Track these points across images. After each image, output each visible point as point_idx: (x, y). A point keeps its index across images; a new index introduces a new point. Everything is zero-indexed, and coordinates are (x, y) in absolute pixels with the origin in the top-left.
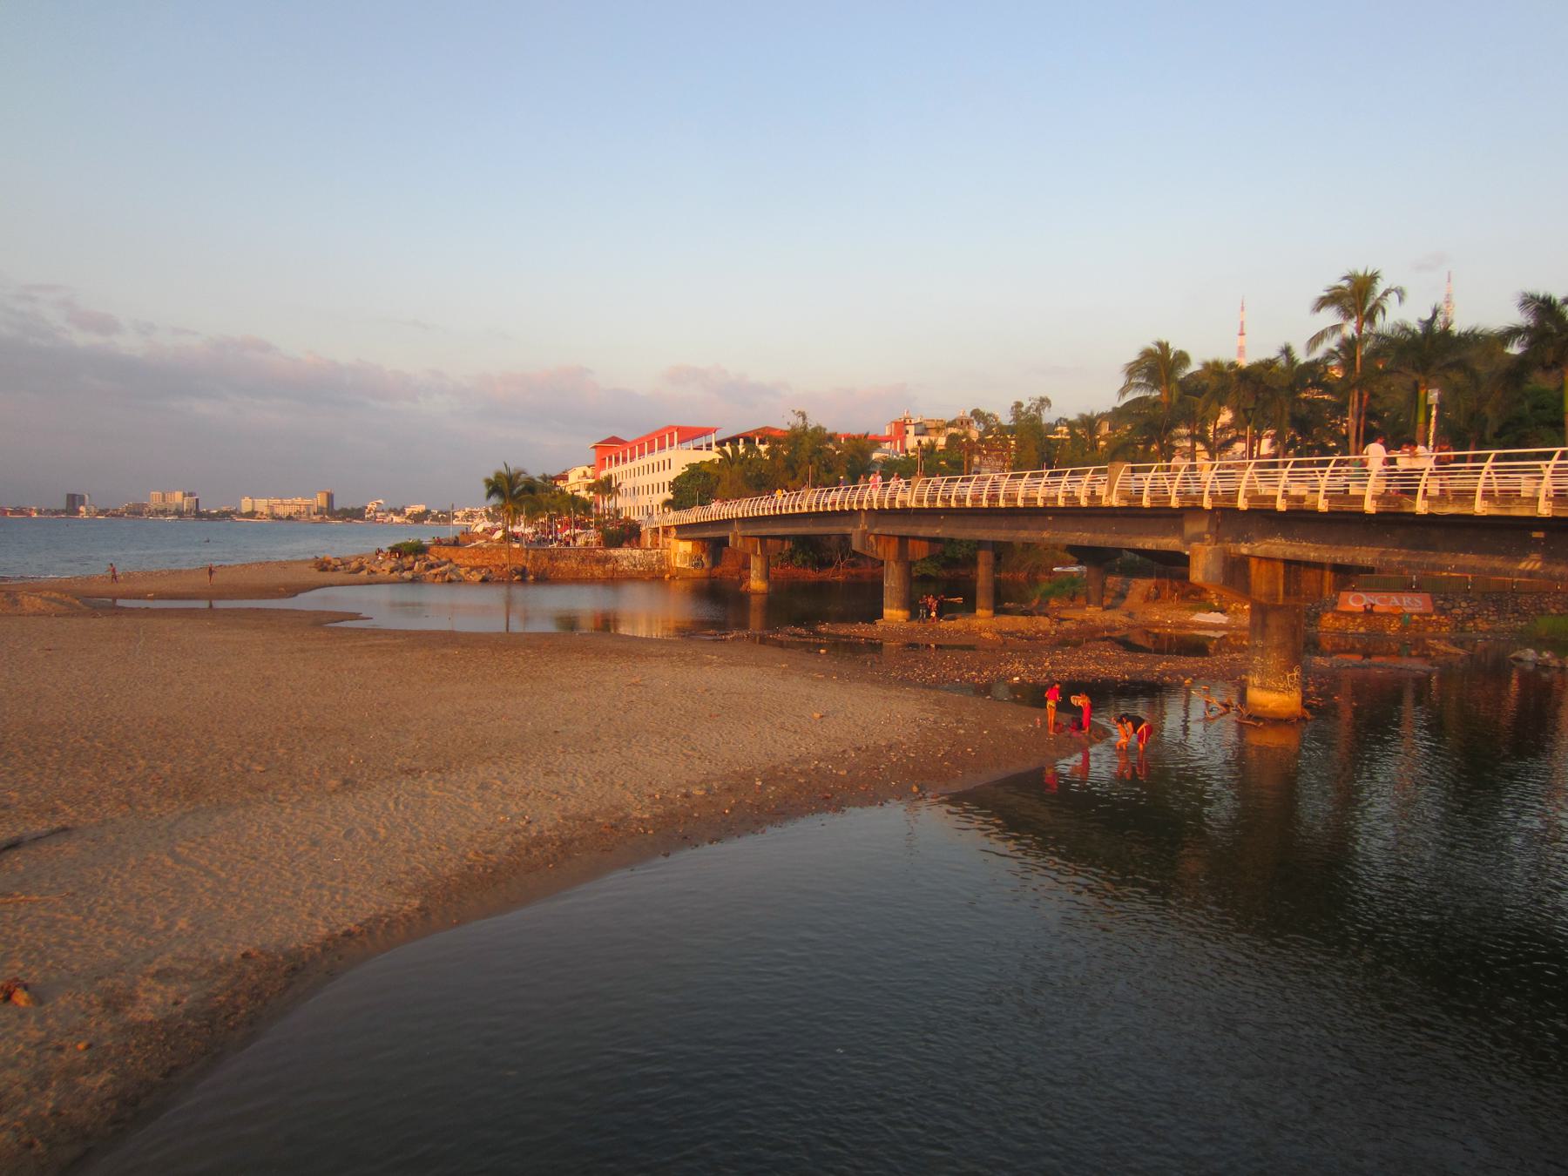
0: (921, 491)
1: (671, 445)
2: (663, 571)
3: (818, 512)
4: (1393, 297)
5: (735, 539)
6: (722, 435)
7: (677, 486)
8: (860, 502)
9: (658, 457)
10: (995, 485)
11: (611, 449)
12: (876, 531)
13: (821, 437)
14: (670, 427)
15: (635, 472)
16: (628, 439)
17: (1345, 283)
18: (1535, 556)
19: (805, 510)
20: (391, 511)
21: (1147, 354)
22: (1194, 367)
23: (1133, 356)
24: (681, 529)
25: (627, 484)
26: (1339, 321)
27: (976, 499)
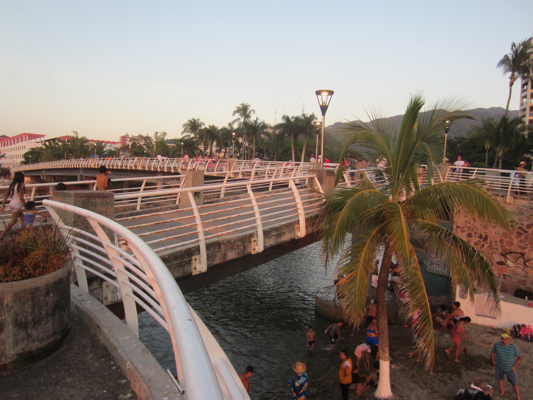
0: (95, 163)
1: (26, 140)
3: (85, 168)
4: (252, 112)
5: (43, 176)
6: (47, 138)
7: (26, 156)
8: (79, 165)
9: (20, 144)
12: (85, 175)
14: (21, 135)
15: (12, 150)
16: (10, 136)
17: (241, 106)
19: (64, 167)
22: (203, 127)
23: (186, 122)
25: (8, 154)
27: (149, 167)
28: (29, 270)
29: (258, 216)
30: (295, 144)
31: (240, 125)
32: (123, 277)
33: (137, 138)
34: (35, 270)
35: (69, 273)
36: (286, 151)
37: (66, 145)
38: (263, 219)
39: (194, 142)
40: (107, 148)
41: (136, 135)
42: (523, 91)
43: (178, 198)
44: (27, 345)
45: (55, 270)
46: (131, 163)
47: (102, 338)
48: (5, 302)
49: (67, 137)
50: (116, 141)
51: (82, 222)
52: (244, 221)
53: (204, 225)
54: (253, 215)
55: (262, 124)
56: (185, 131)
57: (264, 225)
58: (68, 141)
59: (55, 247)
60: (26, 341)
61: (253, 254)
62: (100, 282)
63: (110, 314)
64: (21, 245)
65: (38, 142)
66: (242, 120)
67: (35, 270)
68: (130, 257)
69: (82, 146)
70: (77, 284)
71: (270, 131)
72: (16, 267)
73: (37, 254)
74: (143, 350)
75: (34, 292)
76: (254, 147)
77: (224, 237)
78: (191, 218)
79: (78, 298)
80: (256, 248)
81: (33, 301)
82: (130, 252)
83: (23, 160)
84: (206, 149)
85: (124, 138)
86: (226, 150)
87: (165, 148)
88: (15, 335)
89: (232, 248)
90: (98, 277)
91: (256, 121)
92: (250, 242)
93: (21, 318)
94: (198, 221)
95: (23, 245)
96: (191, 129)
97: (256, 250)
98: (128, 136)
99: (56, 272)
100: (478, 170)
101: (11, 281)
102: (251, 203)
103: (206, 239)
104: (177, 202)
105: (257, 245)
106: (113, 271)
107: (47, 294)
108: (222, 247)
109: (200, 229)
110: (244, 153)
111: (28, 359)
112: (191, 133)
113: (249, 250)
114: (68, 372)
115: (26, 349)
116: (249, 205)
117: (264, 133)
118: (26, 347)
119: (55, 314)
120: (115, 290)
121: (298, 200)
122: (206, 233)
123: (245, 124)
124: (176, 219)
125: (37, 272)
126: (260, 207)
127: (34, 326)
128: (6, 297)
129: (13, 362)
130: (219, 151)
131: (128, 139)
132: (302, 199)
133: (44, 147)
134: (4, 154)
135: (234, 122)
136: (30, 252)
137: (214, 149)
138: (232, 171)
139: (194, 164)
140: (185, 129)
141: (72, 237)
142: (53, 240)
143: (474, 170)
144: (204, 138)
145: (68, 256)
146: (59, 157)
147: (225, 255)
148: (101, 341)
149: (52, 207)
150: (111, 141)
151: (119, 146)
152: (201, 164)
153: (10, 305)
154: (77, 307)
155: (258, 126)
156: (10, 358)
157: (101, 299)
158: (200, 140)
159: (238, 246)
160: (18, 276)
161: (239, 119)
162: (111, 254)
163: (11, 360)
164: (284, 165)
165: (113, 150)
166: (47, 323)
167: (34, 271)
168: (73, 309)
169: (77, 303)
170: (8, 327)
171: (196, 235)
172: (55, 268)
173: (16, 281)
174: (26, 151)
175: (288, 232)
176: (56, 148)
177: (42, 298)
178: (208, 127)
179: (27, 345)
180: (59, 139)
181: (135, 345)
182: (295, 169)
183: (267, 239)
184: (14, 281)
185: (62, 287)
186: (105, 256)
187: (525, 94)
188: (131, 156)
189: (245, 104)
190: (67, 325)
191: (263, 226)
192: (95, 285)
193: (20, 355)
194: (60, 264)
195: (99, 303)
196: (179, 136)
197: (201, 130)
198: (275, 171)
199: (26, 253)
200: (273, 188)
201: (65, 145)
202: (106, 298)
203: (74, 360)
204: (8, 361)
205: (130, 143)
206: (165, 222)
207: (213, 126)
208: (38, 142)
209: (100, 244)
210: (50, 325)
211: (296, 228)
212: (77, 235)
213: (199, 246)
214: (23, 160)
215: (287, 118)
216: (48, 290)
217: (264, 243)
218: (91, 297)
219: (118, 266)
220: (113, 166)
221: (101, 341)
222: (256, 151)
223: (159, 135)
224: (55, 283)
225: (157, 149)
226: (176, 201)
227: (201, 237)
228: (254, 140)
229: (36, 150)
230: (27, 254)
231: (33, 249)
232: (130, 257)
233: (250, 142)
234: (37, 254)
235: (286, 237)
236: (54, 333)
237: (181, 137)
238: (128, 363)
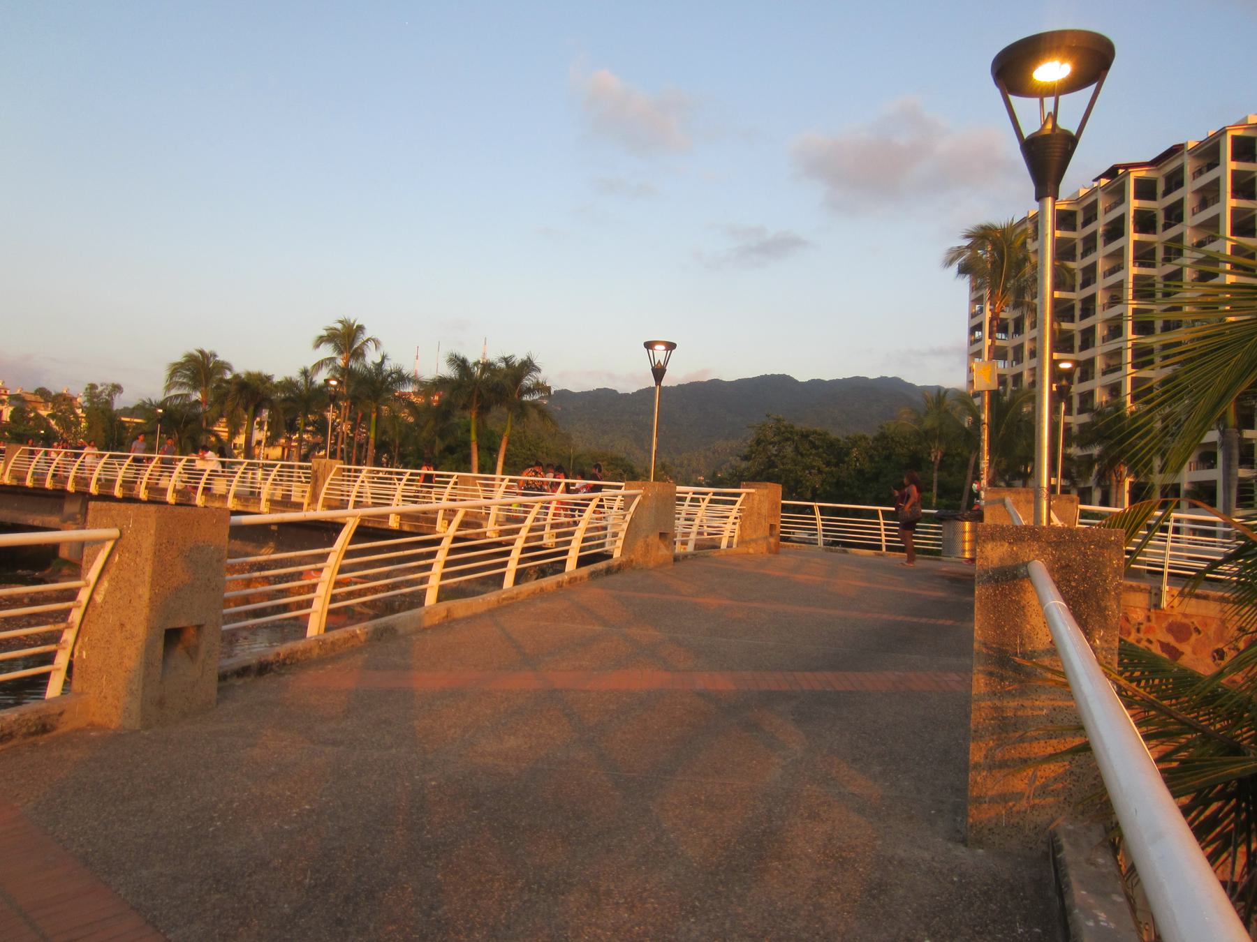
4: (371, 345)
17: (339, 326)
18: (271, 544)
23: (179, 358)
26: (334, 355)
27: (39, 477)
39: (197, 418)
42: (973, 342)
43: (62, 660)
84: (234, 433)
87: (109, 426)
100: (715, 494)
104: (54, 689)
112: (195, 388)
123: (346, 374)
135: (319, 366)
143: (450, 477)
155: (385, 379)
161: (332, 359)
182: (593, 505)
187: (976, 347)
197: (222, 380)
225: (89, 428)
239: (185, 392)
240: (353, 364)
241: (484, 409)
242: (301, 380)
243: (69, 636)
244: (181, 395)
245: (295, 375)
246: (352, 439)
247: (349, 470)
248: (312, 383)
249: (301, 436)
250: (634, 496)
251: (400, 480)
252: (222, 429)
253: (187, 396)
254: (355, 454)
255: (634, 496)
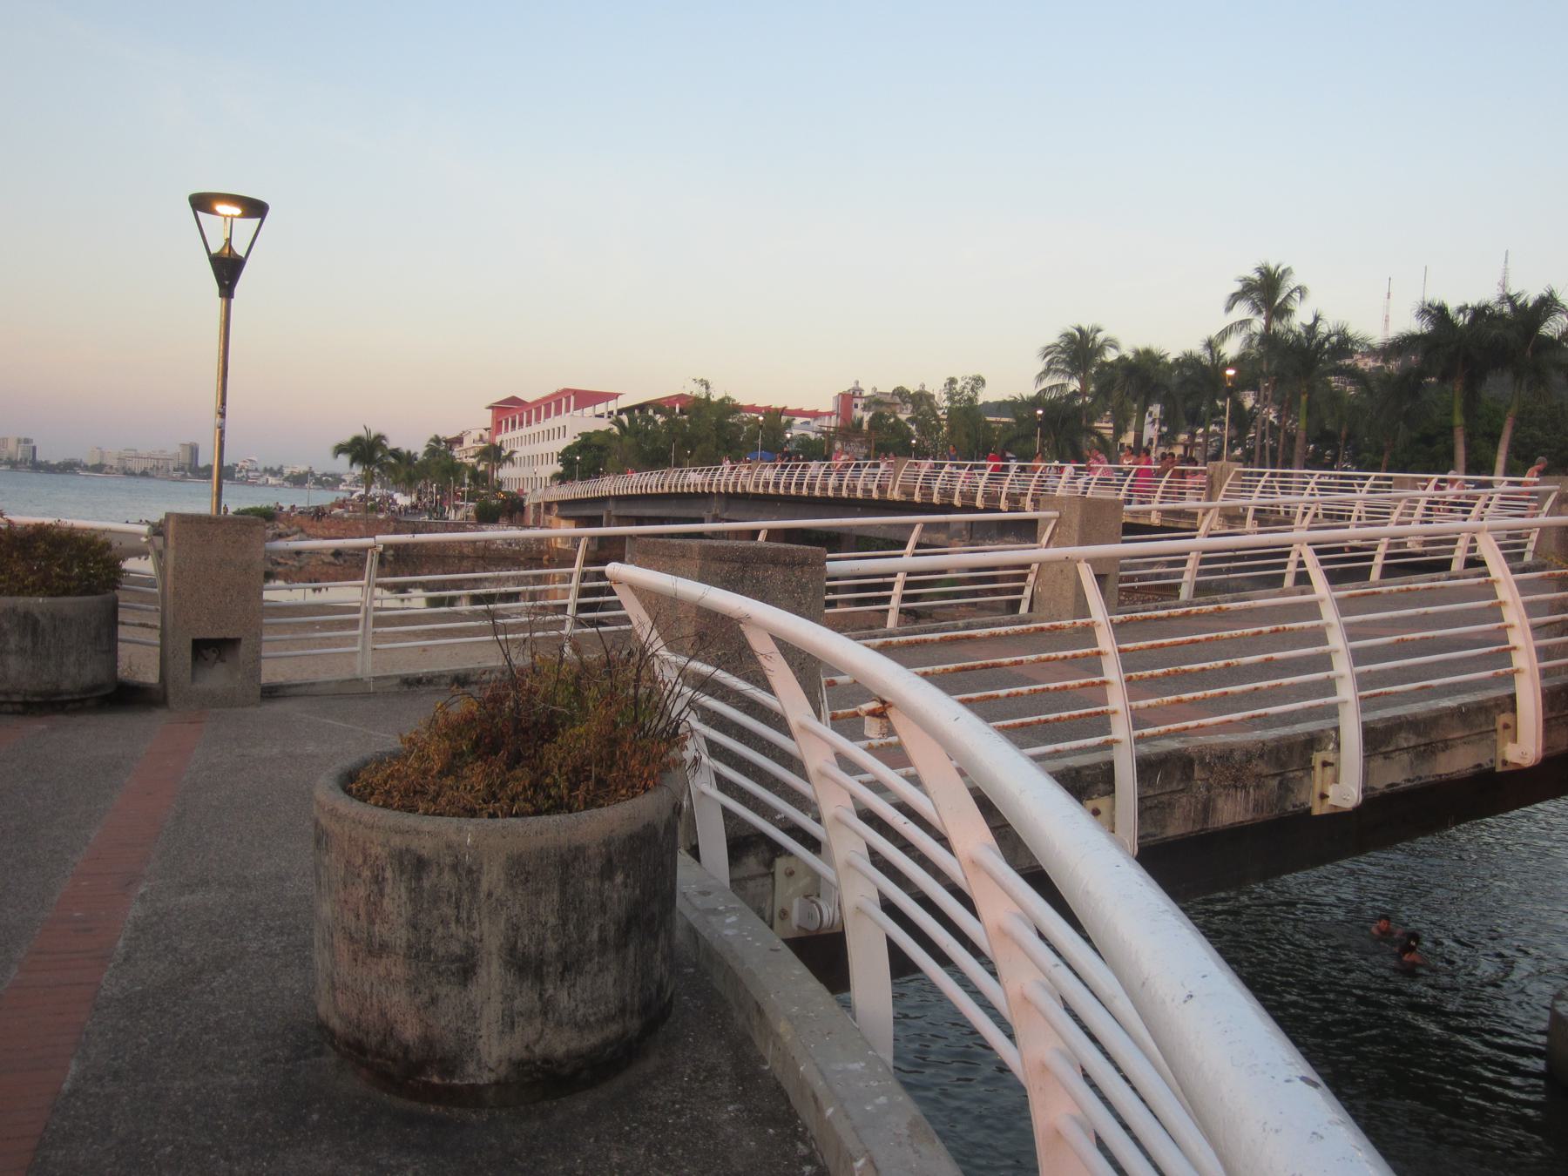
1: (568, 410)
2: (541, 552)
3: (727, 493)
4: (1296, 295)
6: (623, 402)
7: (566, 457)
9: (554, 422)
10: (952, 477)
11: (509, 410)
13: (727, 408)
15: (531, 439)
16: (529, 399)
17: (1256, 276)
19: (666, 490)
20: (266, 470)
21: (1070, 338)
22: (1111, 356)
23: (1053, 338)
24: (563, 504)
25: (522, 451)
28: (555, 784)
29: (1343, 667)
30: (1470, 412)
31: (1249, 346)
32: (849, 844)
33: (888, 399)
34: (573, 787)
35: (677, 809)
36: (1428, 440)
37: (676, 422)
38: (1363, 681)
40: (796, 432)
41: (887, 387)
43: (1027, 593)
44: (541, 1035)
45: (634, 795)
46: (867, 479)
47: (770, 1053)
48: (484, 886)
49: (681, 397)
50: (822, 410)
51: (721, 639)
52: (1286, 681)
53: (1134, 687)
54: (1324, 662)
55: (1334, 339)
56: (1046, 372)
57: (1366, 704)
58: (682, 412)
59: (636, 719)
60: (538, 1023)
61: (1316, 812)
62: (767, 855)
63: (799, 970)
64: (538, 699)
65: (601, 416)
66: (1258, 324)
67: (573, 787)
68: (892, 777)
69: (721, 426)
70: (694, 852)
71: (1367, 364)
72: (518, 772)
73: (580, 737)
74: (913, 1125)
75: (568, 860)
76: (1302, 424)
77: (1202, 739)
78: (1086, 655)
79: (698, 902)
80: (1331, 790)
81: (563, 893)
82: (895, 756)
83: (558, 468)
84: (1119, 431)
85: (847, 399)
86: (1193, 435)
87: (974, 430)
88: (508, 998)
89: (1237, 783)
90: (763, 837)
91: (1311, 330)
92: (1308, 767)
93: (525, 941)
94: (1112, 671)
95: (545, 700)
96: (1069, 363)
97: (1331, 801)
98: (861, 391)
99: (635, 800)
101: (505, 816)
102: (1317, 615)
103: (1140, 740)
104: (1024, 609)
105: (1336, 780)
106: (818, 820)
107: (607, 872)
108: (1197, 775)
109: (1117, 700)
110: (1263, 447)
111: (543, 1081)
113: (1302, 797)
114: (659, 1152)
115: (537, 1050)
116: (1307, 624)
117: (1340, 371)
118: (537, 1042)
119: (626, 945)
120: (815, 888)
121: (1514, 614)
122: (1138, 720)
123: (1269, 339)
124: (1032, 657)
125: (580, 793)
126: (1352, 633)
127: (562, 974)
128: (485, 867)
129: (497, 1083)
130: (1166, 439)
131: (860, 402)
132: (1531, 609)
133: (616, 430)
134: (512, 453)
135: (1225, 334)
136: (563, 725)
137: (1150, 432)
138: (1220, 502)
139: (1080, 483)
140: (1050, 363)
141: (688, 692)
142: (632, 691)
144: (1115, 393)
145: (674, 753)
146: (656, 460)
147: (1207, 808)
148: (765, 1063)
149: (631, 587)
150: (807, 408)
151: (833, 422)
152: (1103, 482)
153: (498, 892)
154: (692, 931)
155: (1321, 344)
156: (491, 1070)
157: (767, 915)
158: (1105, 400)
159: (1259, 776)
160: (526, 800)
161: (1245, 323)
162: (817, 758)
163: (493, 1077)
164: (1425, 489)
165: (812, 436)
166: (600, 970)
167: (571, 791)
168: (680, 935)
169: (692, 917)
170: (489, 965)
171: (1101, 723)
172: (633, 787)
173: (516, 815)
174: (568, 441)
175: (1465, 741)
176: (647, 434)
177: (590, 884)
178: (1131, 356)
179: (541, 1035)
180: (658, 406)
181: (882, 1100)
183: (1378, 761)
184: (511, 816)
185: (655, 851)
186: (793, 763)
188: (867, 457)
189: (1272, 266)
190: (661, 989)
191: (1364, 710)
192: (752, 863)
193: (519, 1065)
194: (651, 775)
195: (764, 927)
196: (1029, 390)
197: (1104, 364)
198: (1398, 510)
199: (549, 728)
200: (1389, 571)
201: (671, 422)
202: (784, 914)
203: (679, 1114)
204: (486, 1078)
205: (867, 416)
206: (994, 666)
207: (1148, 352)
208: (601, 416)
209: (778, 721)
210: (609, 978)
211: (1499, 726)
212: (705, 684)
213: (1111, 764)
214: (558, 468)
215: (1438, 314)
216: (610, 860)
217: (1366, 774)
218: (739, 904)
219: (836, 799)
220: (811, 487)
221: (765, 1063)
222: (1308, 442)
223: (958, 387)
224: (631, 837)
225: (951, 433)
226: (1019, 602)
227: (1121, 730)
228: (1304, 398)
229: (595, 440)
230: (555, 734)
231: (572, 718)
232: (892, 777)
233: (1285, 409)
234: (580, 737)
235: (1458, 761)
236: (622, 1011)
237: (1033, 393)
238: (860, 1164)
239: (1060, 381)
240: (1277, 326)
241: (1473, 382)
242: (1206, 356)
243: (1031, 578)
244: (1056, 386)
245: (1196, 347)
246: (1278, 429)
247: (1251, 474)
248: (1220, 358)
249: (1206, 430)
250: (1549, 493)
251: (1362, 485)
252: (1105, 427)
253: (1063, 385)
254: (1277, 453)
255: (1549, 493)
